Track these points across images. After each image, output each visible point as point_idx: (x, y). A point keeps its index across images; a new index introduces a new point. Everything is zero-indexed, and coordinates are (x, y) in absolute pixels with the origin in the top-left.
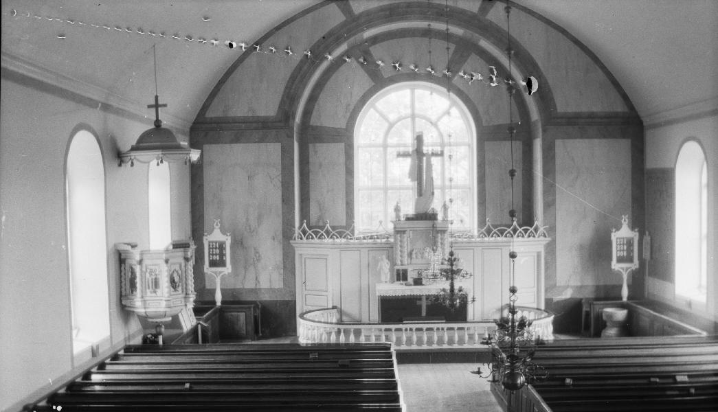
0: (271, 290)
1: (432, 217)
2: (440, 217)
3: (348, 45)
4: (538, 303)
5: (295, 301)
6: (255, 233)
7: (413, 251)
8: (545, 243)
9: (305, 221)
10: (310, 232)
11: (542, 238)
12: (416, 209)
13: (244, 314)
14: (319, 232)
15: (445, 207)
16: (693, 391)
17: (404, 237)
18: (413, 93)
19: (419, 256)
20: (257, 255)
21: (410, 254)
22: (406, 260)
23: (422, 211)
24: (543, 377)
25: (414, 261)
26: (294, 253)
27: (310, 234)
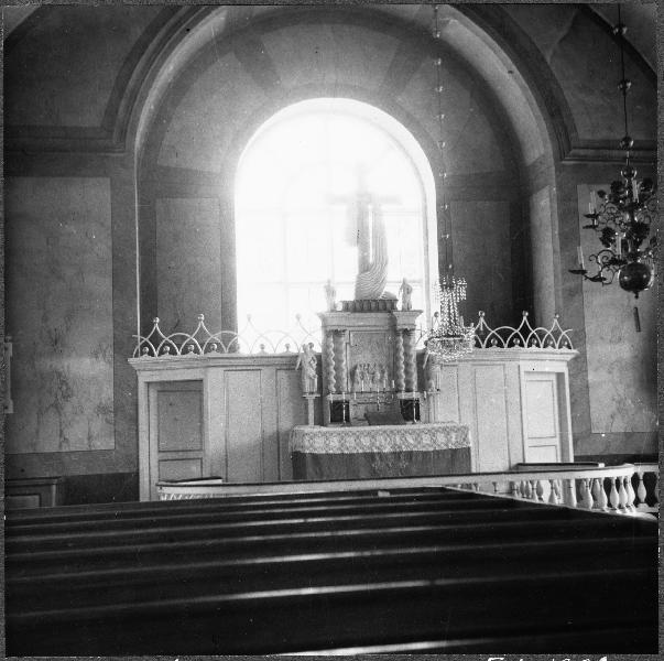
0: (90, 454)
1: (387, 306)
2: (399, 306)
3: (227, 17)
4: (564, 451)
5: (137, 474)
6: (59, 345)
7: (355, 368)
8: (569, 357)
9: (158, 320)
10: (167, 339)
11: (565, 350)
12: (358, 291)
13: (37, 497)
14: (184, 338)
15: (407, 290)
16: (70, 545)
17: (341, 343)
18: (524, 460)
19: (368, 377)
20: (64, 388)
21: (352, 374)
22: (346, 385)
23: (366, 294)
24: (123, 102)
25: (357, 388)
26: (137, 380)
27: (167, 344)
